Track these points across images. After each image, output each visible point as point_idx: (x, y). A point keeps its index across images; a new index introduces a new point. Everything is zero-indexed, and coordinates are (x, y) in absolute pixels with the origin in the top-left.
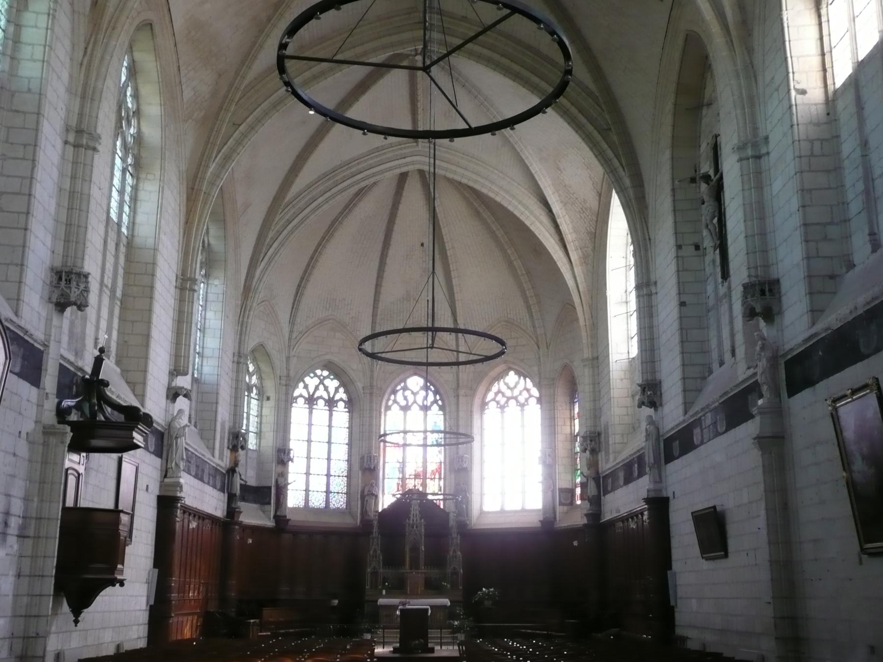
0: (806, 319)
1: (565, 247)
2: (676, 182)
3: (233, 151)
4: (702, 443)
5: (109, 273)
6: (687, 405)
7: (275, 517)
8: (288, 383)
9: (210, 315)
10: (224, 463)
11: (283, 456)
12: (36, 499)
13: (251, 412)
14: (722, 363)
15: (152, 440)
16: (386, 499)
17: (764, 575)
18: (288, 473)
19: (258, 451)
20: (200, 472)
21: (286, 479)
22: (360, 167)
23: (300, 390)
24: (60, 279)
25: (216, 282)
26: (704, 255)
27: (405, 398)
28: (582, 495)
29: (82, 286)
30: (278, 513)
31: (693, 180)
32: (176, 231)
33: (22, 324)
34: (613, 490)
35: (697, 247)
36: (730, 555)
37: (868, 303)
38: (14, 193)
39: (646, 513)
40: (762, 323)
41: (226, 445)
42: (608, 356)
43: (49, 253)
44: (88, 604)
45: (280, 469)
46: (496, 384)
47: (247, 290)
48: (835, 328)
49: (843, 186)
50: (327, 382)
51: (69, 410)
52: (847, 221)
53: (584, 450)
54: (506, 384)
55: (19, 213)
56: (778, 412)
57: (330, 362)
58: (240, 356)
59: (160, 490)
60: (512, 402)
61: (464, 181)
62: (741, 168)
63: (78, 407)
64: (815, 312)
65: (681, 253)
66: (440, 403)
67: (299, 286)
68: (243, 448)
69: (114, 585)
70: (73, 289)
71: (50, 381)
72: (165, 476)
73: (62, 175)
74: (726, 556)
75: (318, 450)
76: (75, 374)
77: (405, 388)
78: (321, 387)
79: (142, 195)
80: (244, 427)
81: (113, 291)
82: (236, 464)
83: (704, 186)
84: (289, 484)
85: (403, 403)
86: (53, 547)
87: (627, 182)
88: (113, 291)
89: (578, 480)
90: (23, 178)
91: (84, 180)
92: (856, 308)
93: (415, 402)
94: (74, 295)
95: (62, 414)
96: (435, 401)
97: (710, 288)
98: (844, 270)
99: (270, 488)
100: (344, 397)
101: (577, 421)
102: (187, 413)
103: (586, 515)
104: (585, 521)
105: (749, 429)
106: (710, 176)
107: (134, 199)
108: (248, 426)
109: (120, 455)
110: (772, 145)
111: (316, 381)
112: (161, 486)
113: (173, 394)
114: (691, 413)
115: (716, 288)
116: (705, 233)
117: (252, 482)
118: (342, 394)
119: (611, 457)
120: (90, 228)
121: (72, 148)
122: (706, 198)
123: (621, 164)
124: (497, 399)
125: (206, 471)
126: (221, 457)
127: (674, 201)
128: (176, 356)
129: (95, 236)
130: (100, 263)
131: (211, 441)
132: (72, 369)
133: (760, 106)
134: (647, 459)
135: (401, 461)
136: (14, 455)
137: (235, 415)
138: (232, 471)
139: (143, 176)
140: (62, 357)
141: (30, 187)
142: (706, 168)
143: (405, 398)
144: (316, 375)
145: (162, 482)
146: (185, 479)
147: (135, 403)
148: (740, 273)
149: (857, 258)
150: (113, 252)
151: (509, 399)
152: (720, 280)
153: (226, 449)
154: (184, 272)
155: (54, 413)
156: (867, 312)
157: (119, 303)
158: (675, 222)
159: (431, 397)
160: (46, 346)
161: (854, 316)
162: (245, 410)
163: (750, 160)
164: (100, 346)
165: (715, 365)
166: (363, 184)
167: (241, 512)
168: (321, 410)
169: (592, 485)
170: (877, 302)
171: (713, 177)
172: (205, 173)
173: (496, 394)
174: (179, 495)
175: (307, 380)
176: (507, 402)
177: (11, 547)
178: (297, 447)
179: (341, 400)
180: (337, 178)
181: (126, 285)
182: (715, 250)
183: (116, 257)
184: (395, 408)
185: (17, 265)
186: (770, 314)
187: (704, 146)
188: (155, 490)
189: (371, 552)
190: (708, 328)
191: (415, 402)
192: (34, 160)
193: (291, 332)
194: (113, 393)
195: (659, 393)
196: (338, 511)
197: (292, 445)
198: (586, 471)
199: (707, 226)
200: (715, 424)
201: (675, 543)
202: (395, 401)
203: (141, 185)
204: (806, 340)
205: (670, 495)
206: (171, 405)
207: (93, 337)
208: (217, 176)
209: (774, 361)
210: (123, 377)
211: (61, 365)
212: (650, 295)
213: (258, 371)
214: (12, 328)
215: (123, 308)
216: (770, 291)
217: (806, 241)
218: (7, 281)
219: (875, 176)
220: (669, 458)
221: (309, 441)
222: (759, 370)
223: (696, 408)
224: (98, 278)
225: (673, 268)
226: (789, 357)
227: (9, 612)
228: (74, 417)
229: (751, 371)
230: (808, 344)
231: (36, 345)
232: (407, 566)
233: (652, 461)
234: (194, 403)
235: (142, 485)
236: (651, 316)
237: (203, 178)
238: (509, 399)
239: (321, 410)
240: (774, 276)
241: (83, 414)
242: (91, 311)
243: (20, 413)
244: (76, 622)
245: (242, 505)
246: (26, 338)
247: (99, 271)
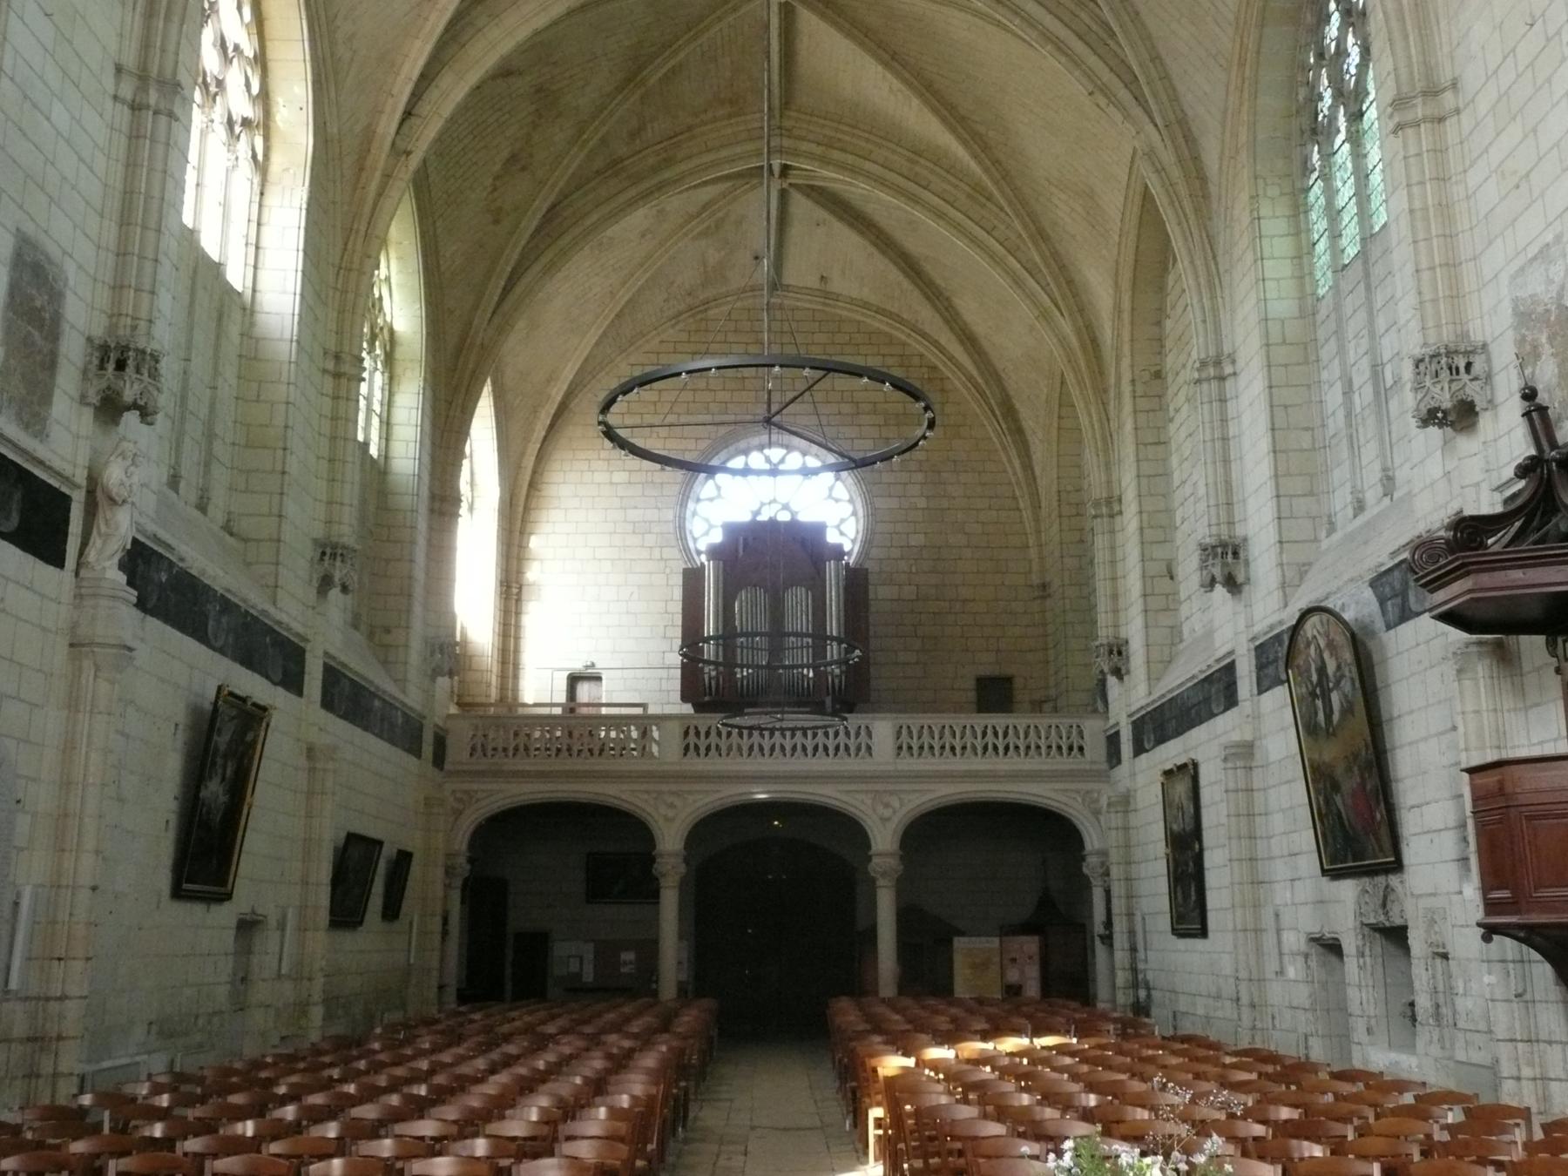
64: (1152, 679)
110: (1241, 363)
121: (331, 379)
133: (1438, 23)
163: (1422, 126)
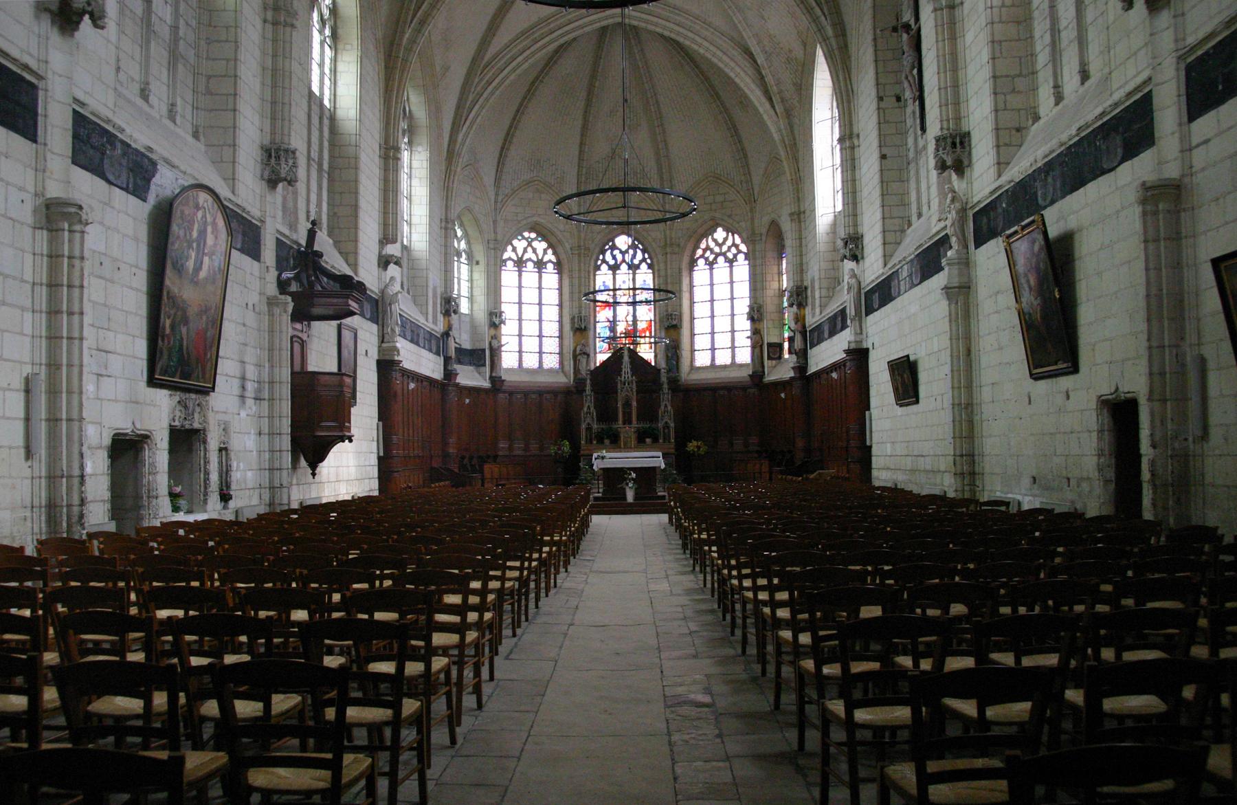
0: (993, 171)
1: (770, 100)
2: (878, 31)
3: (428, 15)
4: (899, 295)
5: (315, 147)
6: (886, 257)
7: (491, 377)
8: (496, 247)
9: (415, 182)
10: (440, 328)
11: (495, 320)
12: (267, 365)
13: (462, 277)
14: (920, 215)
15: (367, 307)
16: (602, 356)
17: (946, 417)
18: (501, 335)
19: (471, 316)
20: (415, 335)
21: (500, 342)
22: (558, 22)
23: (509, 253)
24: (270, 156)
25: (420, 149)
26: (905, 106)
27: (614, 257)
28: (789, 349)
29: (291, 162)
30: (494, 375)
31: (895, 29)
32: (376, 99)
33: (239, 202)
34: (818, 343)
35: (898, 99)
36: (920, 401)
37: (1046, 156)
38: (222, 76)
39: (848, 364)
40: (954, 177)
41: (439, 310)
42: (814, 210)
43: (258, 132)
44: (322, 459)
45: (493, 332)
46: (704, 241)
47: (451, 155)
48: (1017, 180)
49: (1032, 37)
50: (535, 244)
51: (288, 281)
52: (1034, 73)
53: (791, 305)
54: (715, 241)
55: (227, 95)
56: (965, 263)
57: (537, 223)
58: (447, 222)
59: (379, 355)
60: (721, 259)
61: (666, 33)
62: (936, 20)
63: (297, 278)
64: (1001, 165)
65: (883, 105)
66: (649, 261)
67: (502, 148)
68: (455, 312)
69: (343, 441)
70: (283, 166)
71: (269, 253)
72: (383, 342)
73: (264, 53)
74: (917, 402)
75: (530, 312)
76: (291, 248)
77: (614, 247)
78: (530, 249)
79: (341, 67)
80: (456, 292)
81: (320, 165)
82: (450, 328)
83: (905, 36)
84: (502, 346)
85: (612, 262)
86: (286, 407)
87: (830, 31)
88: (320, 165)
89: (786, 335)
90: (228, 60)
91: (284, 57)
92: (1036, 161)
93: (624, 261)
94: (284, 170)
95: (282, 286)
96: (644, 260)
97: (910, 141)
98: (1030, 122)
99: (484, 350)
100: (553, 259)
101: (785, 277)
102: (399, 280)
103: (793, 368)
104: (792, 374)
105: (938, 281)
106: (910, 26)
107: (334, 71)
108: (459, 290)
109: (338, 322)
111: (524, 243)
112: (379, 351)
113: (384, 262)
114: (889, 266)
115: (916, 139)
116: (906, 85)
117: (467, 345)
118: (550, 256)
119: (818, 311)
120: (293, 103)
122: (906, 48)
123: (824, 14)
124: (706, 255)
125: (421, 336)
126: (435, 322)
127: (875, 51)
128: (385, 225)
129: (299, 113)
130: (306, 139)
131: (424, 307)
132: (288, 242)
134: (848, 312)
135: (611, 319)
136: (244, 325)
137: (446, 281)
138: (446, 334)
139: (340, 46)
140: (278, 231)
141: (235, 68)
142: (907, 17)
143: (614, 257)
144: (524, 238)
145: (379, 347)
146: (402, 344)
147: (349, 272)
148: (934, 129)
149: (1042, 111)
150: (318, 126)
151: (717, 255)
152: (919, 132)
153: (439, 314)
154: (386, 141)
155: (275, 285)
156: (1045, 165)
157: (326, 175)
158: (877, 73)
159: (639, 256)
160: (263, 222)
161: (1034, 168)
162: (456, 275)
164: (312, 218)
165: (914, 218)
166: (562, 41)
167: (457, 374)
168: (530, 276)
169: (798, 338)
170: (1054, 155)
171: (913, 26)
172: (401, 39)
173: (705, 251)
174: (396, 358)
175: (515, 242)
176: (715, 259)
177: (250, 408)
178: (509, 311)
179: (550, 261)
180: (536, 35)
181: (331, 157)
182: (914, 102)
183: (321, 131)
184: (604, 267)
185: (230, 146)
186: (960, 167)
188: (374, 354)
189: (585, 409)
190: (908, 181)
191: (624, 261)
192: (236, 42)
193: (497, 195)
194: (327, 263)
195: (860, 247)
196: (551, 370)
197: (504, 307)
198: (793, 326)
199: (907, 78)
200: (910, 276)
201: (873, 392)
202: (604, 261)
203: (339, 57)
204: (992, 193)
205: (870, 347)
206: (383, 273)
207: (304, 210)
208: (413, 41)
209: (963, 211)
210: (336, 247)
211: (277, 239)
212: (853, 148)
213: (466, 235)
214: (231, 206)
215: (331, 180)
216: (962, 143)
217: (995, 94)
218: (222, 161)
219: (1061, 28)
220: (870, 310)
221: (520, 303)
222: (949, 223)
223: (895, 260)
224: (305, 153)
225: (874, 119)
226: (977, 209)
227: (255, 466)
228: (294, 287)
229: (942, 224)
230: (993, 197)
231: (254, 221)
232: (620, 422)
233: (853, 313)
234: (405, 270)
235: (361, 350)
236: (854, 168)
237: (399, 45)
238: (717, 255)
239: (530, 276)
240: (965, 129)
241: (302, 284)
242: (301, 186)
243: (245, 287)
244: (314, 475)
245: (458, 367)
246: (244, 215)
247: (305, 145)
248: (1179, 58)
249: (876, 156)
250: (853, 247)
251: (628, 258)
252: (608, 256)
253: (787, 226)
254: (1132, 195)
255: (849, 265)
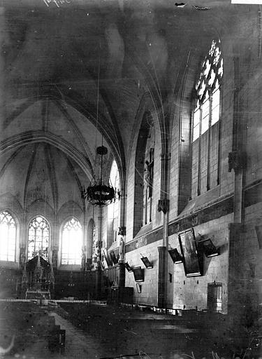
0: (176, 214)
16: (30, 257)
77: (36, 221)
114: (181, 215)
159: (45, 225)
165: (144, 224)
169: (98, 258)
187: (147, 152)
248: (256, 193)
249: (133, 203)
250: (123, 231)
251: (41, 225)
252: (34, 224)
253: (96, 220)
254: (227, 225)
255: (121, 236)
